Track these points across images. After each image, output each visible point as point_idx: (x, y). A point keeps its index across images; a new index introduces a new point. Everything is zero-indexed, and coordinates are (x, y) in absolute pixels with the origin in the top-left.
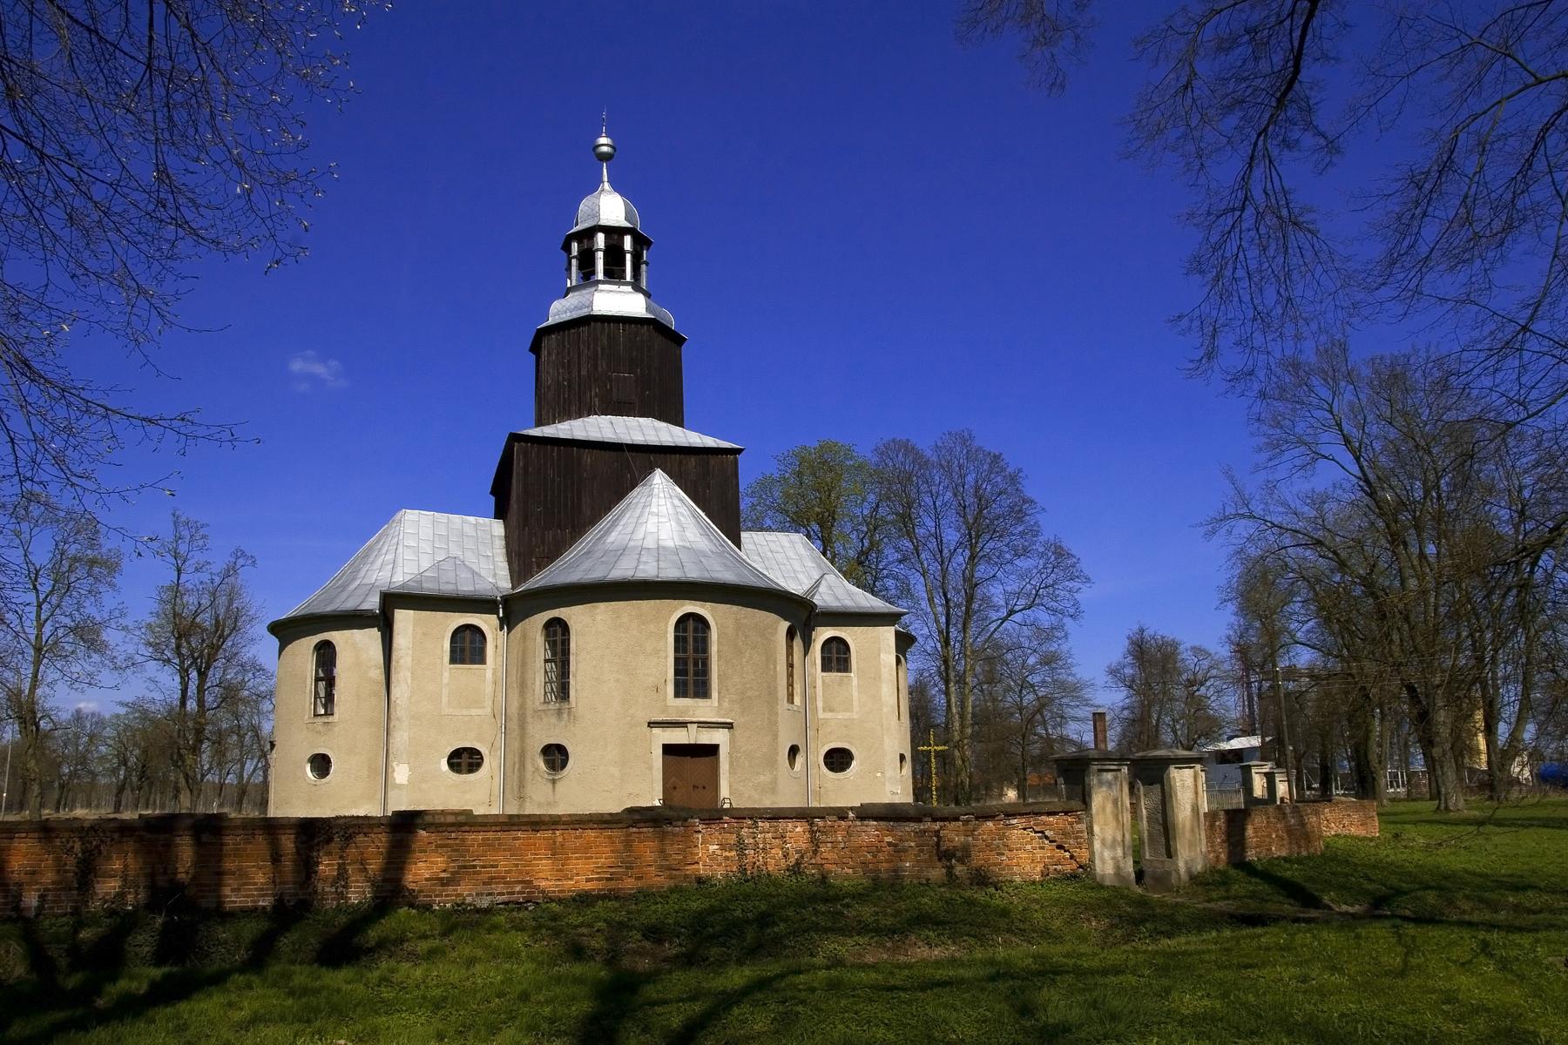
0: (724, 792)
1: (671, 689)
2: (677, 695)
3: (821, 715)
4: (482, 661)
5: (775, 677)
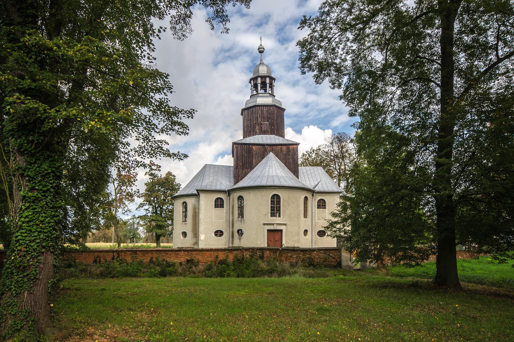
0: (284, 242)
1: (269, 215)
2: (271, 216)
3: (317, 221)
4: (223, 207)
5: (299, 211)
